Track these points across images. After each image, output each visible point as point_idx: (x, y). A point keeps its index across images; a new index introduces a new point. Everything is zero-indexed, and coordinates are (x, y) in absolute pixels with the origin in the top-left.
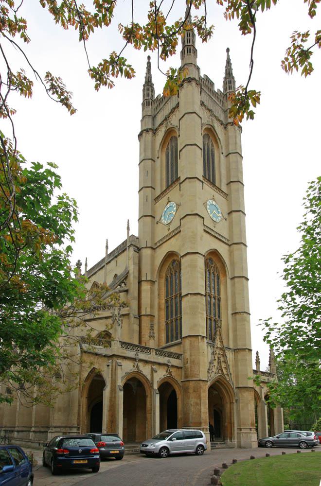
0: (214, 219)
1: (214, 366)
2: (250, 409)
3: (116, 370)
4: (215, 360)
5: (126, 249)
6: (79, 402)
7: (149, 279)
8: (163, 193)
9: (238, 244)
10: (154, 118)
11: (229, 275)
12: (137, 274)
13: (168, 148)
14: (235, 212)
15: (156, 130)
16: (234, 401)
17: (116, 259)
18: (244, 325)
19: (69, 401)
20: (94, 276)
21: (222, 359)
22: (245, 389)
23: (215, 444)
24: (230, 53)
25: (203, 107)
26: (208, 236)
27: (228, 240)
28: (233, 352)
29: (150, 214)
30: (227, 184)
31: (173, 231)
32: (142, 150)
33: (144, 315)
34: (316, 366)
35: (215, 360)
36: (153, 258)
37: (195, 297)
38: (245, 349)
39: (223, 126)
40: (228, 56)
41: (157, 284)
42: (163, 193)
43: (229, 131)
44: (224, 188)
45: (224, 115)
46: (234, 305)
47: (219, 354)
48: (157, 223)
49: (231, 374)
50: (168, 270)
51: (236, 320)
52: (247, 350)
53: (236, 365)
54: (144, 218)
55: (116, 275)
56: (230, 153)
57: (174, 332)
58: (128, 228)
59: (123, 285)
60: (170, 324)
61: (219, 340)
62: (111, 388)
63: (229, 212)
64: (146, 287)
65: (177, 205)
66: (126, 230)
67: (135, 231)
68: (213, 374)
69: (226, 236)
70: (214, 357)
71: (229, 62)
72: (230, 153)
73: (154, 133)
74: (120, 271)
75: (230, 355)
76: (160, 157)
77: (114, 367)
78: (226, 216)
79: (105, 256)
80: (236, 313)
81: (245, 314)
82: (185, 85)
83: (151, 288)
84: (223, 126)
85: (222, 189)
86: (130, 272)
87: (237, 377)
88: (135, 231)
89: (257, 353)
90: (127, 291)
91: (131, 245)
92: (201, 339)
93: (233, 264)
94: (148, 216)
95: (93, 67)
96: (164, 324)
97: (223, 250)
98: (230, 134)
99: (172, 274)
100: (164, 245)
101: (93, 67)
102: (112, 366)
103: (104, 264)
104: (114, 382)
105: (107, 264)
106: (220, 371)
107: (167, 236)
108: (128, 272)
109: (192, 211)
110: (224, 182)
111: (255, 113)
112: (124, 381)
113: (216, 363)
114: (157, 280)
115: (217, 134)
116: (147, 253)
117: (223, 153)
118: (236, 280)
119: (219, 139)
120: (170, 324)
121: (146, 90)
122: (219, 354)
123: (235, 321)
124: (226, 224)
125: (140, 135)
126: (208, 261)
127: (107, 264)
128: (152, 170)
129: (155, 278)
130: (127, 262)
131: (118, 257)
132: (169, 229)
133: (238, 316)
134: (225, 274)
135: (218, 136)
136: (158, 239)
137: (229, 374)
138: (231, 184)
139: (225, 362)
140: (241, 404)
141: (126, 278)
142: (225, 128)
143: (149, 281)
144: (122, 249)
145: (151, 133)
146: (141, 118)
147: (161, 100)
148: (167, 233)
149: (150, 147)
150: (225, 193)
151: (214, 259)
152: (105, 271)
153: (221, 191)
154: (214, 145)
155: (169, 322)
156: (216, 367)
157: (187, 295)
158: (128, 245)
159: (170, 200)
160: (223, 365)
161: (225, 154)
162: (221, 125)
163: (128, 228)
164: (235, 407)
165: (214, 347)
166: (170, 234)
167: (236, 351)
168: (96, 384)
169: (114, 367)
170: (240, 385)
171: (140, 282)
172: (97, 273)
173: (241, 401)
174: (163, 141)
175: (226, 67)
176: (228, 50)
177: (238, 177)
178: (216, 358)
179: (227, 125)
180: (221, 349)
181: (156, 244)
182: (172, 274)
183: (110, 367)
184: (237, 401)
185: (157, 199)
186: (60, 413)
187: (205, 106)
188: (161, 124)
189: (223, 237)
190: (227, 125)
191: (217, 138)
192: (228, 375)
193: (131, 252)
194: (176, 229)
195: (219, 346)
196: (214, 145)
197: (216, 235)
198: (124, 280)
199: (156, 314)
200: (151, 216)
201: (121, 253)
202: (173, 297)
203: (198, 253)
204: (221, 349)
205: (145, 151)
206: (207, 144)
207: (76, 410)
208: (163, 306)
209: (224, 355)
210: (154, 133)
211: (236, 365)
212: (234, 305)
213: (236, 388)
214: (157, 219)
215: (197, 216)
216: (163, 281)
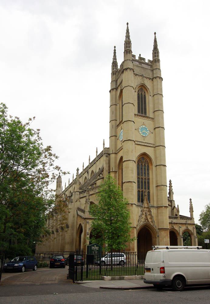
0: (144, 135)
1: (143, 218)
2: (165, 241)
3: (86, 225)
4: (143, 214)
5: (102, 156)
6: (76, 239)
7: (114, 171)
9: (159, 146)
10: (116, 81)
11: (154, 164)
12: (107, 169)
14: (159, 128)
15: (117, 88)
16: (157, 237)
17: (100, 159)
18: (162, 192)
19: (73, 239)
20: (92, 167)
21: (148, 213)
22: (162, 229)
27: (154, 144)
28: (156, 209)
32: (111, 97)
34: (102, 237)
35: (143, 214)
36: (116, 158)
37: (128, 183)
38: (162, 206)
39: (151, 80)
40: (155, 37)
41: (118, 172)
43: (154, 82)
44: (151, 115)
45: (152, 73)
46: (157, 181)
47: (146, 211)
49: (154, 221)
51: (157, 190)
52: (164, 207)
53: (157, 216)
54: (112, 137)
55: (99, 169)
56: (155, 95)
58: (104, 144)
59: (101, 175)
61: (146, 203)
62: (84, 233)
63: (154, 128)
66: (103, 145)
67: (107, 145)
68: (142, 222)
69: (152, 142)
70: (143, 213)
71: (155, 41)
72: (155, 95)
74: (101, 167)
75: (154, 211)
77: (86, 224)
78: (152, 131)
79: (103, 150)
80: (157, 186)
81: (162, 186)
82: (124, 72)
83: (115, 175)
84: (151, 80)
86: (105, 168)
87: (158, 223)
88: (107, 145)
89: (170, 181)
90: (103, 178)
91: (106, 153)
92: (131, 205)
93: (156, 158)
94: (114, 136)
97: (149, 151)
98: (154, 84)
100: (120, 152)
102: (85, 223)
103: (82, 175)
104: (85, 231)
105: (97, 161)
106: (146, 221)
108: (104, 168)
109: (127, 138)
112: (90, 230)
113: (144, 216)
115: (145, 85)
116: (113, 156)
118: (158, 167)
119: (148, 88)
122: (146, 211)
123: (157, 190)
124: (152, 135)
125: (110, 92)
126: (141, 159)
127: (97, 161)
128: (115, 110)
129: (117, 170)
130: (102, 163)
131: (101, 159)
133: (158, 188)
134: (152, 164)
135: (147, 87)
136: (118, 148)
137: (153, 221)
138: (155, 112)
139: (150, 215)
140: (160, 239)
141: (102, 171)
143: (113, 171)
144: (99, 157)
145: (115, 90)
146: (111, 82)
149: (114, 98)
150: (152, 118)
151: (145, 157)
152: (96, 165)
153: (149, 118)
154: (146, 92)
156: (144, 218)
157: (124, 182)
158: (103, 153)
160: (149, 217)
161: (152, 95)
163: (104, 144)
164: (157, 240)
165: (142, 207)
167: (158, 207)
169: (86, 224)
170: (160, 228)
171: (109, 172)
172: (93, 166)
173: (160, 237)
176: (155, 33)
178: (144, 213)
179: (153, 78)
180: (147, 208)
181: (117, 151)
183: (84, 224)
184: (158, 236)
185: (118, 126)
186: (68, 245)
187: (138, 75)
188: (119, 86)
189: (150, 144)
190: (153, 78)
191: (147, 89)
192: (152, 222)
193: (104, 158)
195: (146, 206)
197: (145, 144)
198: (101, 173)
200: (115, 136)
204: (147, 208)
205: (112, 101)
207: (75, 244)
209: (150, 211)
210: (117, 90)
211: (157, 216)
212: (157, 181)
213: (158, 229)
214: (118, 137)
215: (129, 141)
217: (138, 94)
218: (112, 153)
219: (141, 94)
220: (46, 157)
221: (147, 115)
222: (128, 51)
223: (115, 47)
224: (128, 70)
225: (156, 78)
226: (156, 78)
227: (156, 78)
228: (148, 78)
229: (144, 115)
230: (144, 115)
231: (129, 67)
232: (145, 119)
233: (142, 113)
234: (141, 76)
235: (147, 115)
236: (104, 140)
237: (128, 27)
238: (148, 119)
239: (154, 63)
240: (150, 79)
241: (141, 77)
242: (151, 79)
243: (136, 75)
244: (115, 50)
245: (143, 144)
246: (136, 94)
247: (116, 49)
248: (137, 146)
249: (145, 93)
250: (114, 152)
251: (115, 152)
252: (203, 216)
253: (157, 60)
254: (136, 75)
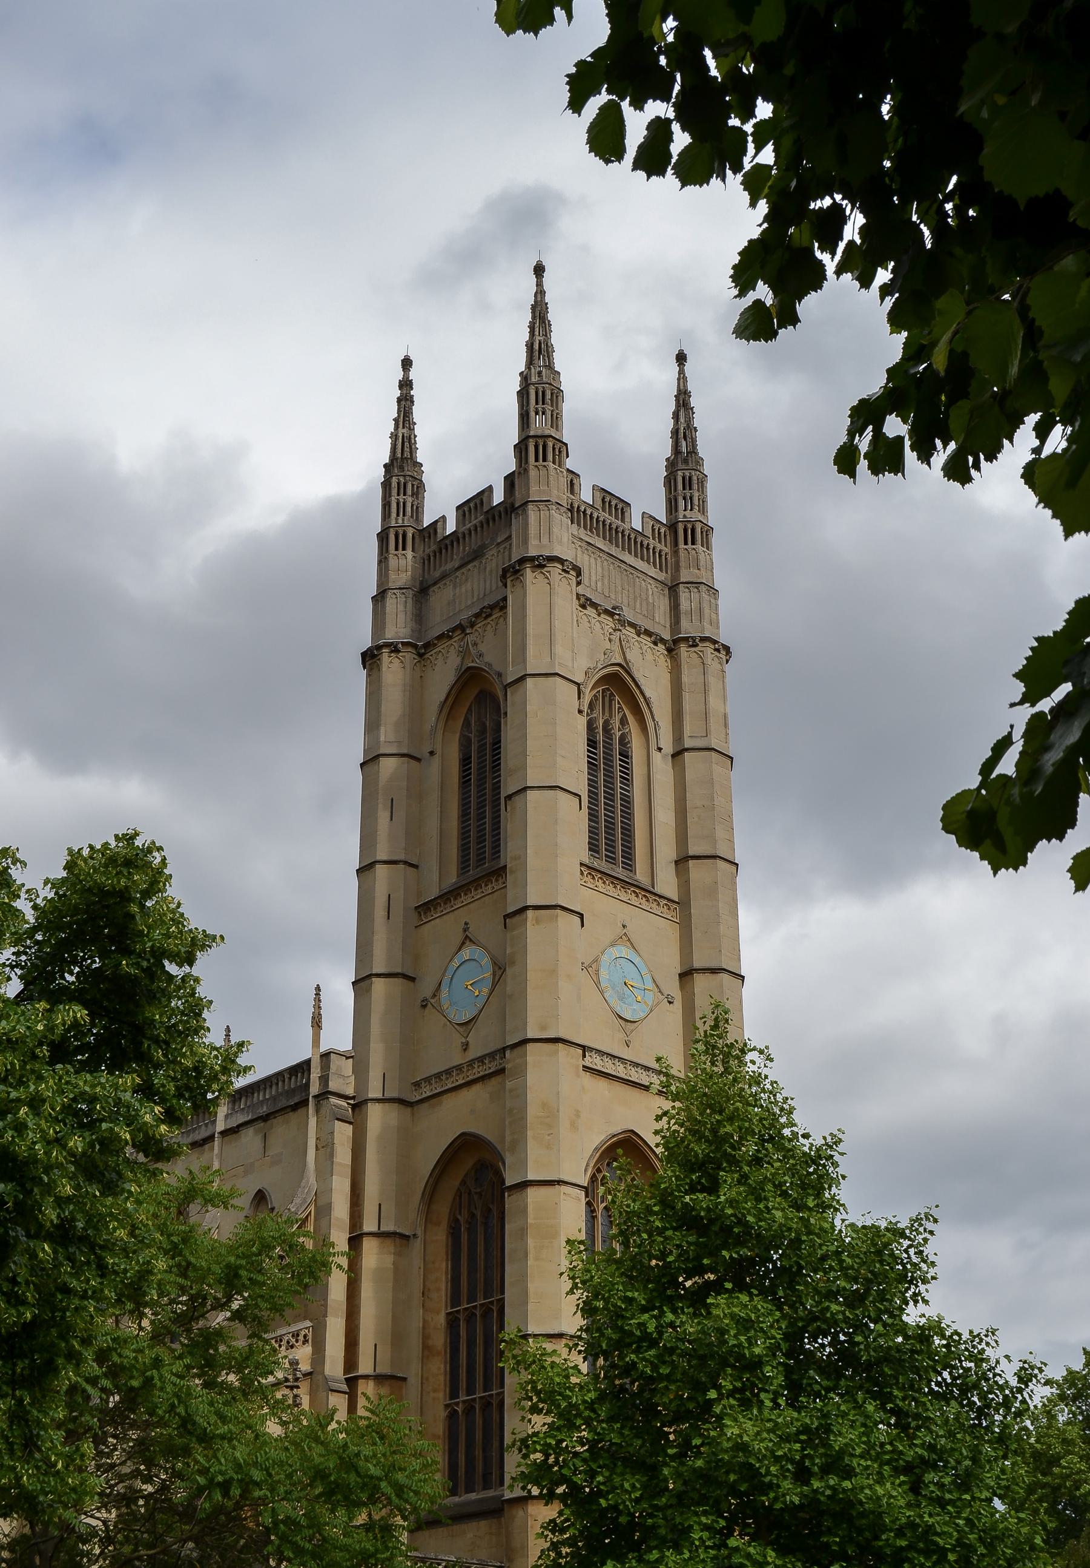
8: (448, 896)
13: (467, 724)
23: (665, 542)
24: (688, 367)
25: (591, 611)
26: (602, 1084)
29: (399, 970)
30: (673, 756)
31: (481, 1060)
33: (366, 1377)
39: (661, 647)
40: (682, 377)
41: (418, 1244)
42: (448, 896)
44: (667, 883)
48: (424, 1006)
50: (459, 1194)
56: (687, 750)
57: (478, 1453)
58: (317, 1022)
60: (462, 1418)
64: (372, 1254)
65: (495, 964)
71: (683, 400)
73: (421, 655)
76: (439, 752)
78: (673, 987)
84: (661, 647)
85: (658, 890)
95: (753, 204)
96: (442, 1414)
99: (473, 1216)
101: (753, 204)
107: (459, 1068)
109: (543, 1028)
110: (666, 851)
111: (664, 177)
114: (419, 1232)
117: (660, 749)
120: (462, 1418)
121: (394, 492)
132: (466, 1047)
142: (670, 651)
145: (408, 656)
147: (448, 542)
148: (458, 1059)
153: (651, 897)
155: (459, 1409)
159: (473, 931)
162: (655, 643)
163: (317, 1022)
166: (471, 1063)
168: (693, 543)
174: (451, 700)
175: (676, 416)
177: (712, 839)
179: (676, 642)
182: (473, 1216)
185: (425, 908)
187: (594, 605)
190: (676, 642)
194: (492, 1055)
196: (630, 718)
199: (413, 1373)
200: (404, 976)
201: (283, 1110)
202: (459, 1409)
203: (560, 1182)
206: (606, 723)
208: (439, 1340)
216: (440, 1235)
217: (591, 726)
218: (378, 1100)
219: (607, 730)
220: (292, 1347)
221: (641, 875)
222: (550, 444)
223: (407, 363)
224: (555, 569)
225: (692, 642)
226: (695, 645)
227: (692, 642)
228: (648, 633)
229: (620, 872)
230: (620, 872)
231: (557, 552)
232: (634, 900)
233: (611, 860)
234: (611, 614)
235: (641, 875)
236: (318, 988)
237: (540, 292)
238: (645, 905)
239: (682, 546)
240: (658, 640)
241: (609, 622)
242: (662, 641)
243: (585, 603)
244: (406, 385)
245: (620, 1071)
246: (582, 722)
247: (412, 375)
248: (587, 1077)
249: (624, 722)
250: (388, 1095)
251: (403, 1096)
252: (161, 1090)
253: (698, 526)
254: (583, 607)
